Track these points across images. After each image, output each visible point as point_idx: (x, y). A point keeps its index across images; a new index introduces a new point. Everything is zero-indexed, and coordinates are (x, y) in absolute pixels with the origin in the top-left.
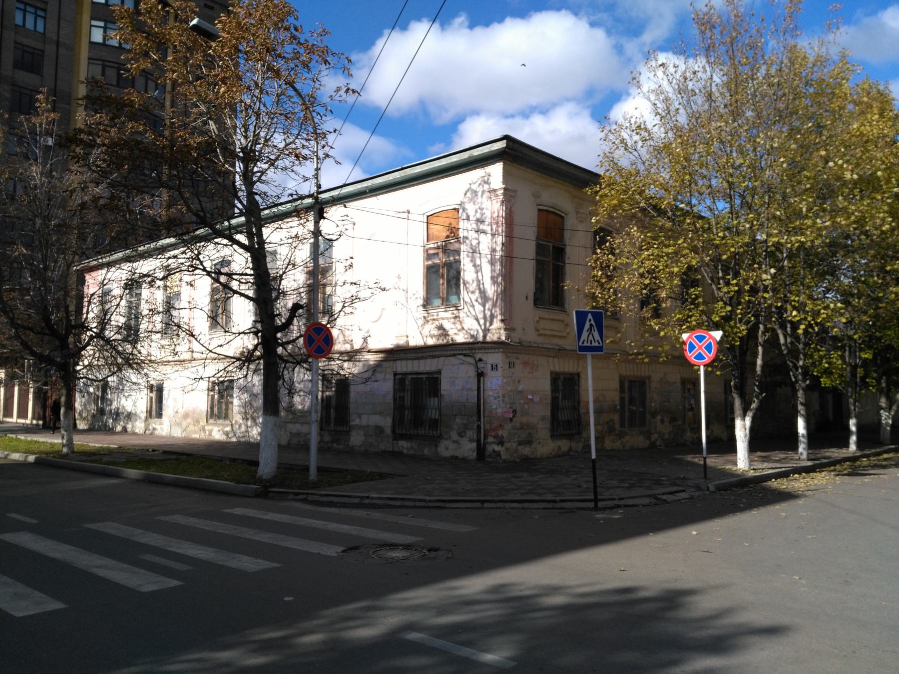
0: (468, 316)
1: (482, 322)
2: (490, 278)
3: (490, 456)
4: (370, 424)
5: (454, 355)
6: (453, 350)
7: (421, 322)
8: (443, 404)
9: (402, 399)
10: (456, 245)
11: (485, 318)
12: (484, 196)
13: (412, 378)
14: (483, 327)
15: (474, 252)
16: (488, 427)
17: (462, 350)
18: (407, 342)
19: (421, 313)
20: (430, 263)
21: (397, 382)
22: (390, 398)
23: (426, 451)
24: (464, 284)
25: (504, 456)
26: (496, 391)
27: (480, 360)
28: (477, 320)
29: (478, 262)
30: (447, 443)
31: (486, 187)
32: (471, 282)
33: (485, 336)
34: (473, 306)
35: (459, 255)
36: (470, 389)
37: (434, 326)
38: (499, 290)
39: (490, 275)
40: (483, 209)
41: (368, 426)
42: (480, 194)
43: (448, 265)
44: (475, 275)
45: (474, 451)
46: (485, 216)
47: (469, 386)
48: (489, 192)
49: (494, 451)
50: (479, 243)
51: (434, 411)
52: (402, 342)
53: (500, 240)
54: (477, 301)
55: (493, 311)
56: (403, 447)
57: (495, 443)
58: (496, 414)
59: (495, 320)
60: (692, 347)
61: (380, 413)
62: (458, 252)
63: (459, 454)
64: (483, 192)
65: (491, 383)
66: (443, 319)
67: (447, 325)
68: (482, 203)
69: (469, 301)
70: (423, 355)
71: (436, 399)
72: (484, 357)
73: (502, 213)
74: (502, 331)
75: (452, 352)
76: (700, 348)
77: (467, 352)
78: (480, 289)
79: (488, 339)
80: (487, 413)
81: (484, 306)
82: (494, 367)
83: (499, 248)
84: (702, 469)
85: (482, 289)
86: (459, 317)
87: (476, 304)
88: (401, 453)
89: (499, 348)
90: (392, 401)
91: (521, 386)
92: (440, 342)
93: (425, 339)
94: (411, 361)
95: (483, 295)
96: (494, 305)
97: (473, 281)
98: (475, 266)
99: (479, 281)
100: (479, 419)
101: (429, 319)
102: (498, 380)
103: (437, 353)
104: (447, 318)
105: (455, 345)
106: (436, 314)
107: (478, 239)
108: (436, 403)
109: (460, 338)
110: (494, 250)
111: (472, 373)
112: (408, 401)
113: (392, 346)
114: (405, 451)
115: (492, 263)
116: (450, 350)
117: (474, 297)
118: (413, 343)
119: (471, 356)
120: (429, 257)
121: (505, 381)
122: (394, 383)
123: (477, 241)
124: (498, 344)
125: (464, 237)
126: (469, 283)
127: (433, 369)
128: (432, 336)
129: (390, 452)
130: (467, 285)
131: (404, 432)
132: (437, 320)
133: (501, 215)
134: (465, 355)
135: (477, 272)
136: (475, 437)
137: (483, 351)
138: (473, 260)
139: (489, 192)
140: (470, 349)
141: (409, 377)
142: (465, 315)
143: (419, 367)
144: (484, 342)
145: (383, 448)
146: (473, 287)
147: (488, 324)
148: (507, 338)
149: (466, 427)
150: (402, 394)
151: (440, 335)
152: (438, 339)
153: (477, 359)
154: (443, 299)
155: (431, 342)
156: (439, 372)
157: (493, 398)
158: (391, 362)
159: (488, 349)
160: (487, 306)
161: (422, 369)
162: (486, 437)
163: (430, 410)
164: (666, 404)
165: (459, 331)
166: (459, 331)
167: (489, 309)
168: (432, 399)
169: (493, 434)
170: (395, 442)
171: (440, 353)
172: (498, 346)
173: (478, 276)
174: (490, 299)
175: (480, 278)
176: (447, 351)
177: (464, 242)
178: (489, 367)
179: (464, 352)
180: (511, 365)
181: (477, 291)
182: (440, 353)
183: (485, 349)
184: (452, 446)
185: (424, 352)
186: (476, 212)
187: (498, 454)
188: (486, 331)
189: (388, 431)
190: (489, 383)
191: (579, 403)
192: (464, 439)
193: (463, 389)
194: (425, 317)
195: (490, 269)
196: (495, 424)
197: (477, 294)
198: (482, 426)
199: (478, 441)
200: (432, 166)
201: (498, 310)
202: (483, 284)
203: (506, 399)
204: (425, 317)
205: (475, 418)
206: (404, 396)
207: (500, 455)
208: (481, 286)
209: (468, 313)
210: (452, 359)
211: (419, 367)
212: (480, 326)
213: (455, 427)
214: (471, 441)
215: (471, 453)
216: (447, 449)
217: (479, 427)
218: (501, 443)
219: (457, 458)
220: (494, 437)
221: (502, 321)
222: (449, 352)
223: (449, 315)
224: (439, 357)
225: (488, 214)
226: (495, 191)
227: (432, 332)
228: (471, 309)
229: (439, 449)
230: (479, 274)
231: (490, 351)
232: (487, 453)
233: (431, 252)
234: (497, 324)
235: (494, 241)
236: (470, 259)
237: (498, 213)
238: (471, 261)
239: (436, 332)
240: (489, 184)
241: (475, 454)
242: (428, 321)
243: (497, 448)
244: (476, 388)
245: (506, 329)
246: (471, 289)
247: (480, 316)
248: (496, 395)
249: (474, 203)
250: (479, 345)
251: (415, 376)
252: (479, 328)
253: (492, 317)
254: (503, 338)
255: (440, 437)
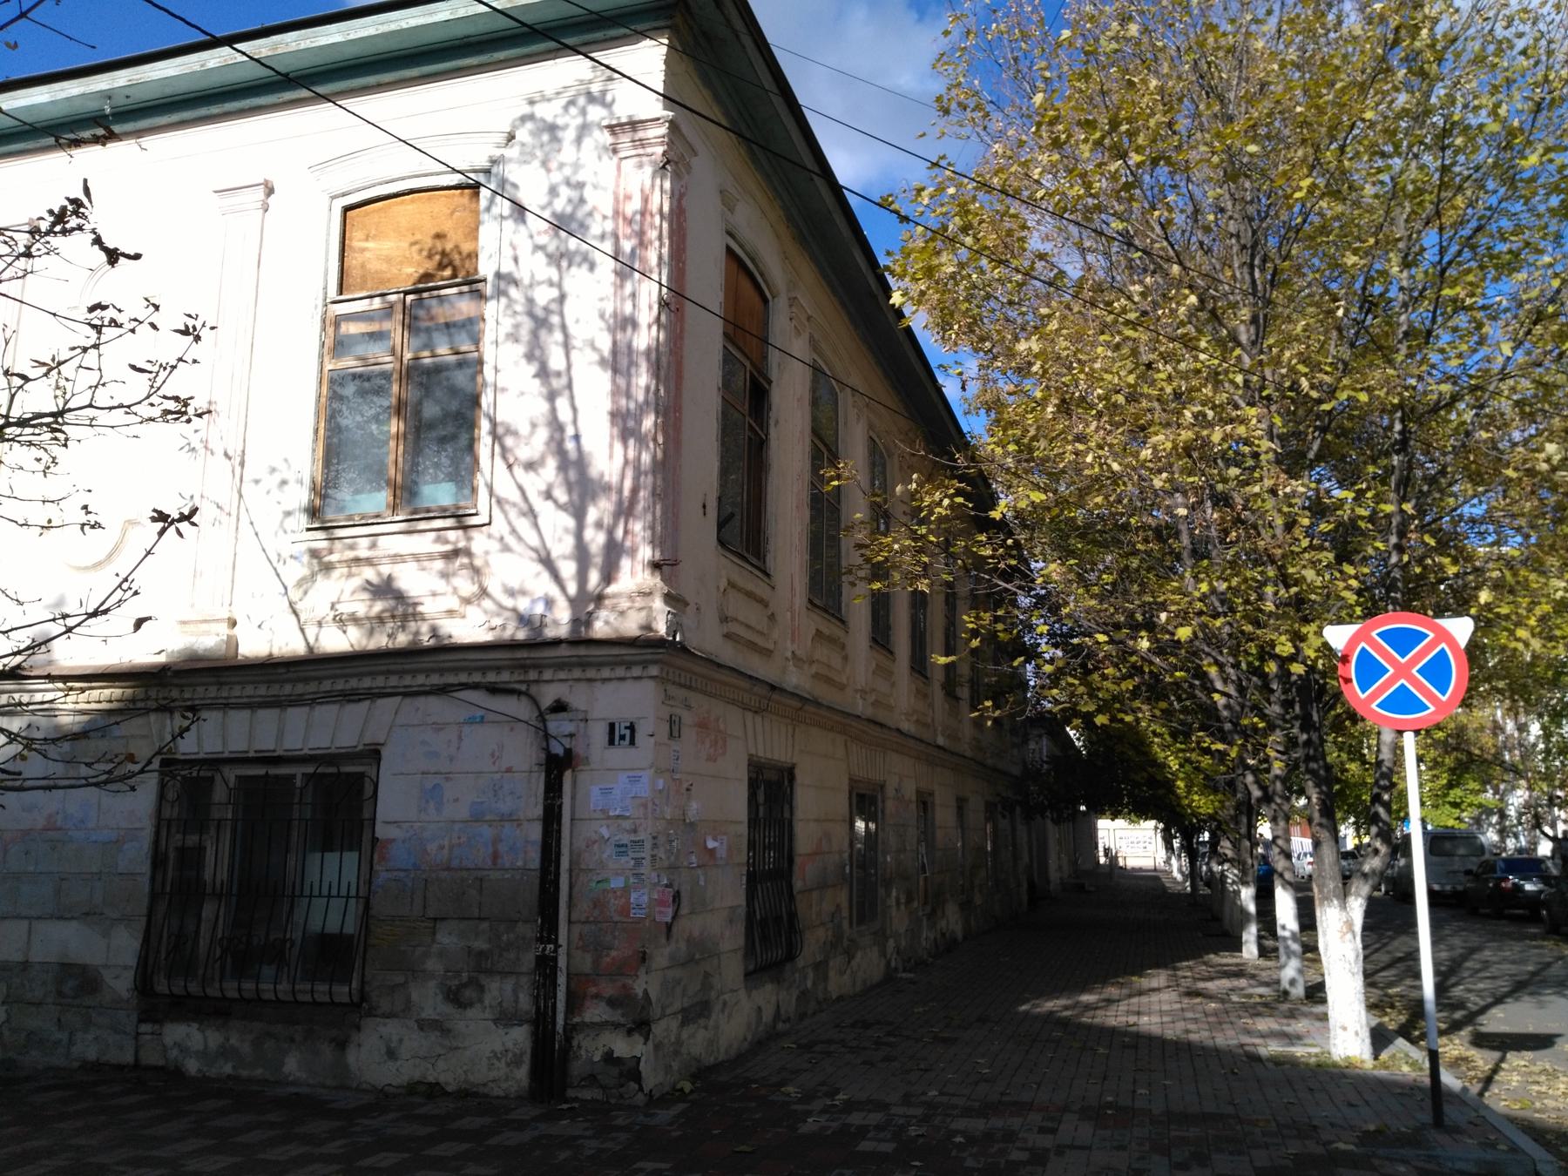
0: (506, 548)
1: (568, 569)
2: (605, 420)
3: (592, 1079)
4: (36, 956)
5: (443, 690)
6: (442, 671)
7: (295, 571)
8: (382, 876)
9: (191, 858)
10: (465, 307)
11: (582, 554)
12: (588, 142)
13: (238, 778)
14: (572, 588)
15: (540, 323)
16: (585, 963)
17: (484, 670)
18: (232, 643)
19: (299, 537)
20: (348, 363)
21: (171, 795)
22: (136, 856)
23: (292, 1065)
24: (494, 433)
25: (652, 1077)
26: (627, 824)
27: (560, 707)
28: (547, 562)
29: (556, 361)
30: (391, 1029)
31: (596, 113)
32: (524, 429)
33: (581, 620)
34: (531, 514)
35: (476, 340)
36: (510, 818)
37: (357, 582)
38: (646, 458)
39: (606, 405)
40: (580, 186)
41: (25, 965)
42: (569, 136)
43: (421, 376)
44: (544, 406)
45: (516, 1062)
46: (587, 208)
47: (505, 806)
48: (611, 128)
49: (609, 1057)
50: (562, 298)
51: (337, 904)
52: (208, 640)
53: (649, 293)
54: (548, 495)
55: (619, 533)
56: (184, 1050)
57: (616, 1026)
58: (625, 910)
59: (625, 563)
60: (1370, 670)
61: (89, 915)
62: (471, 327)
63: (446, 1073)
64: (584, 130)
65: (606, 792)
66: (397, 558)
67: (411, 581)
68: (577, 166)
69: (515, 496)
70: (300, 688)
71: (351, 858)
72: (577, 697)
73: (660, 201)
74: (658, 604)
75: (435, 680)
76: (1402, 671)
77: (505, 676)
78: (561, 452)
79: (601, 627)
80: (583, 908)
81: (579, 515)
82: (621, 734)
83: (646, 313)
84: (1428, 1103)
85: (573, 455)
86: (468, 553)
87: (544, 509)
88: (174, 1074)
89: (645, 664)
90: (145, 868)
91: (694, 805)
92: (380, 641)
93: (311, 632)
94: (246, 714)
95: (572, 475)
96: (625, 511)
97: (534, 426)
98: (543, 373)
99: (556, 426)
100: (549, 929)
101: (334, 558)
102: (634, 780)
103: (367, 683)
104: (417, 558)
105: (445, 652)
106: (365, 542)
107: (560, 286)
108: (350, 874)
109: (470, 628)
110: (626, 323)
111: (521, 753)
112: (217, 863)
113: (162, 659)
114: (192, 1066)
115: (618, 362)
116: (428, 672)
117: (534, 483)
118: (253, 646)
119: (519, 693)
120: (339, 346)
121: (660, 784)
122: (161, 796)
123: (555, 293)
124: (644, 646)
125: (499, 276)
126: (515, 434)
127: (347, 739)
128: (341, 622)
129: (120, 1067)
130: (509, 441)
131: (194, 988)
132: (369, 562)
133: (654, 205)
134: (494, 690)
135: (552, 397)
136: (525, 1003)
137: (577, 673)
138: (535, 353)
139: (611, 128)
140: (524, 667)
141: (231, 774)
142: (495, 546)
143: (280, 735)
144: (580, 640)
145: (92, 1054)
146: (534, 445)
147: (594, 577)
148: (673, 627)
149: (483, 965)
150: (192, 840)
151: (380, 619)
152: (371, 632)
153: (547, 701)
154: (395, 489)
155: (335, 641)
156: (373, 754)
157: (609, 850)
158: (153, 717)
159: (599, 665)
160: (592, 514)
161: (294, 742)
162: (574, 1003)
163: (319, 903)
164: (1389, 871)
165: (467, 601)
166: (467, 601)
167: (599, 525)
168: (332, 858)
169: (609, 989)
170: (144, 1028)
171: (380, 681)
172: (648, 654)
173: (553, 410)
174: (607, 488)
175: (564, 414)
176: (414, 673)
177: (500, 293)
178: (599, 733)
179: (491, 677)
180: (674, 727)
181: (552, 463)
182: (380, 681)
183: (583, 664)
184: (413, 1042)
185: (306, 680)
186: (553, 191)
187: (631, 1071)
188: (586, 603)
189: (121, 984)
190: (595, 791)
191: (791, 861)
192: (470, 1013)
193: (477, 817)
194: (314, 554)
195: (608, 386)
196: (619, 951)
197: (550, 470)
198: (562, 962)
199: (541, 1023)
200: (393, 27)
201: (637, 527)
202: (577, 437)
203: (661, 853)
204: (314, 554)
205: (528, 930)
206: (201, 849)
207: (636, 1076)
208: (570, 446)
209: (511, 540)
210: (434, 705)
211: (280, 735)
212: (563, 588)
213: (432, 965)
214: (505, 1018)
215: (501, 1068)
216: (391, 1054)
217: (546, 966)
218: (641, 1026)
219: (434, 1091)
220: (612, 1003)
221: (655, 566)
222: (421, 679)
223: (424, 543)
224: (373, 695)
225: (600, 201)
226: (634, 125)
227: (346, 609)
228: (523, 525)
229: (352, 1057)
230: (562, 404)
231: (606, 673)
232: (577, 1068)
233: (353, 328)
234: (634, 576)
235: (628, 288)
236: (521, 349)
237: (646, 200)
238: (530, 357)
239: (361, 606)
240: (608, 106)
241: (522, 1074)
242: (328, 568)
243: (622, 1047)
244: (539, 811)
245: (669, 598)
246: (524, 453)
247: (562, 547)
248: (626, 839)
249: (544, 164)
250: (563, 651)
251: (259, 771)
252: (554, 591)
253: (614, 552)
254: (661, 628)
255: (360, 1008)
